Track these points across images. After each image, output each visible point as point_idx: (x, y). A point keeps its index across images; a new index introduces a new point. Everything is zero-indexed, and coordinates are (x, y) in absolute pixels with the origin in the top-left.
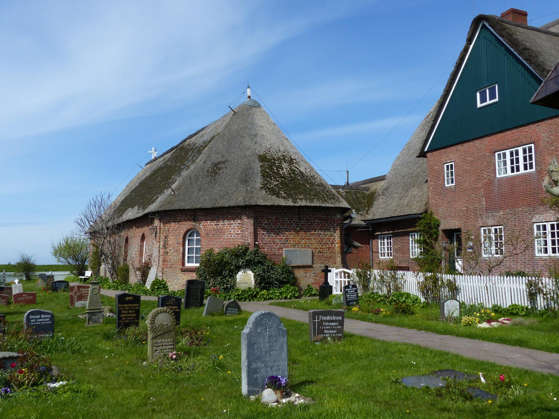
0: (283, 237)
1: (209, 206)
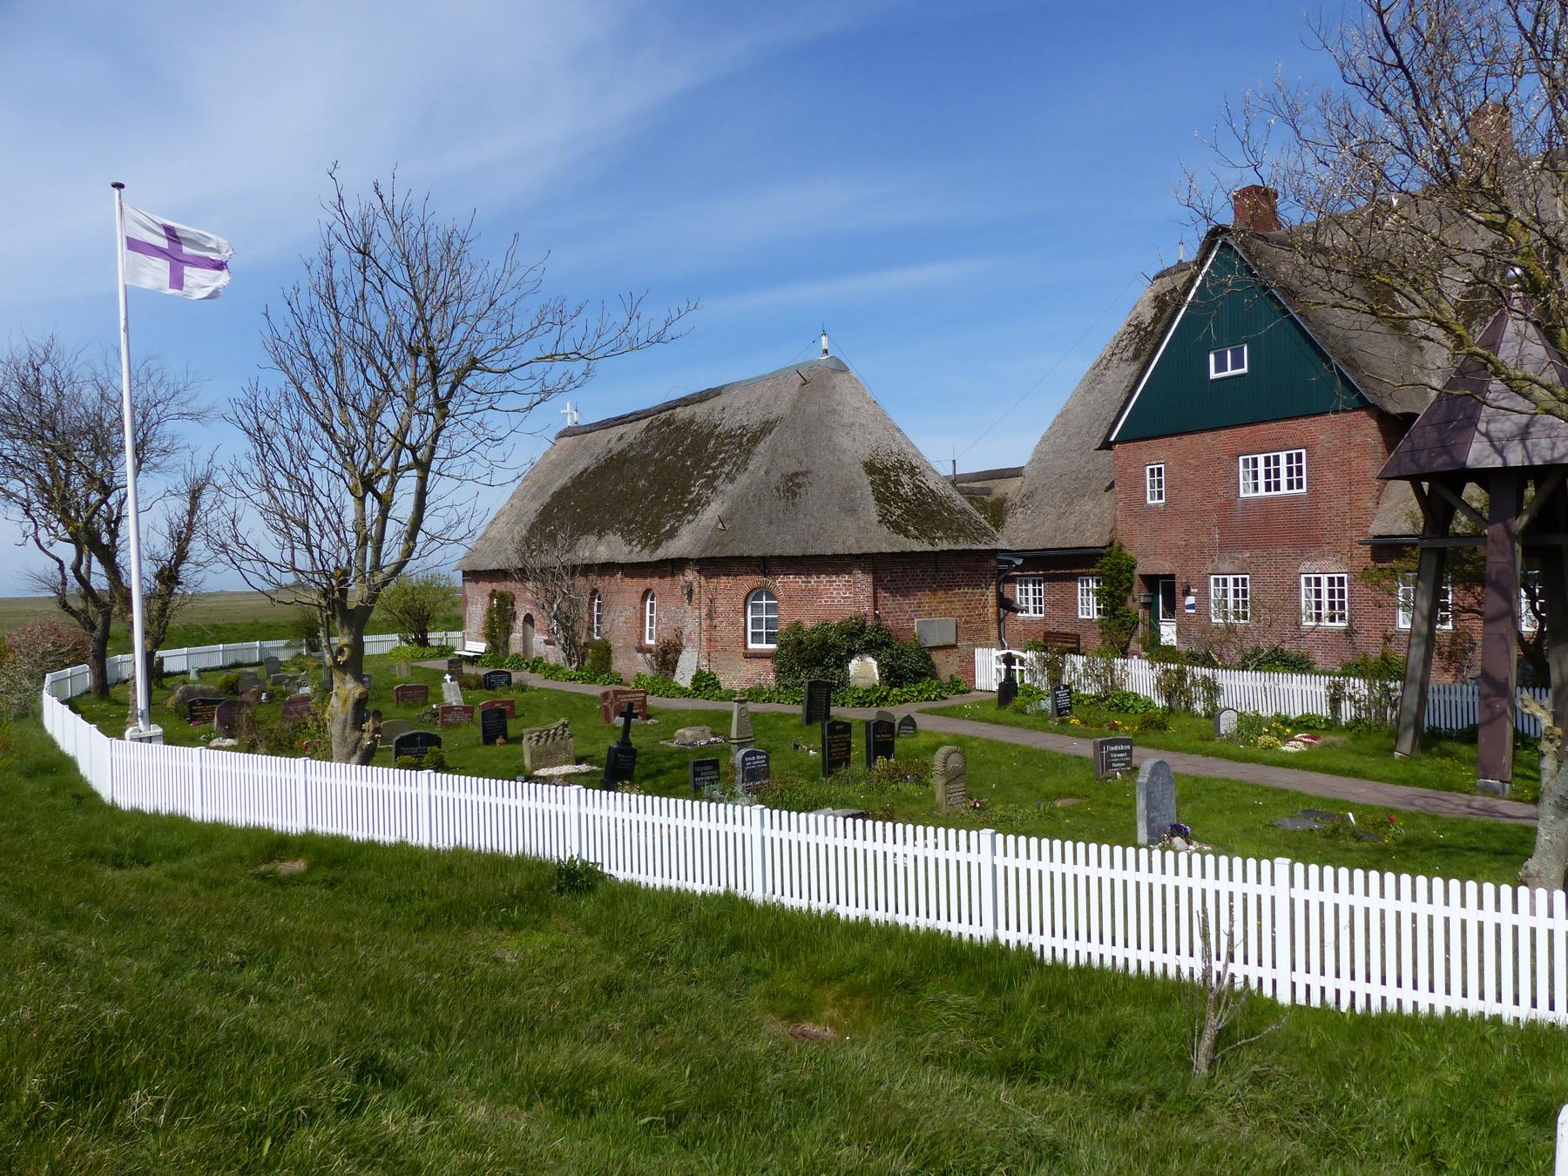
0: (913, 600)
1: (798, 552)
